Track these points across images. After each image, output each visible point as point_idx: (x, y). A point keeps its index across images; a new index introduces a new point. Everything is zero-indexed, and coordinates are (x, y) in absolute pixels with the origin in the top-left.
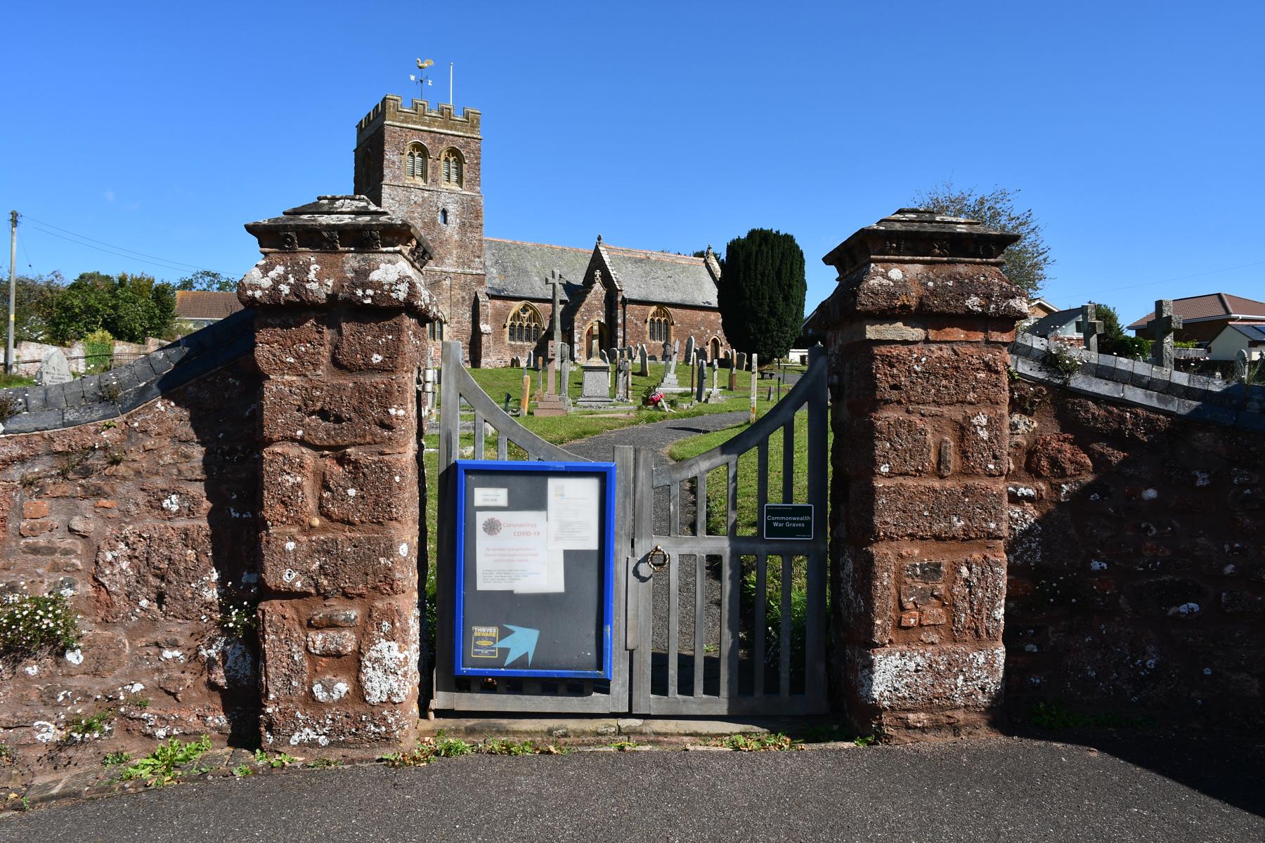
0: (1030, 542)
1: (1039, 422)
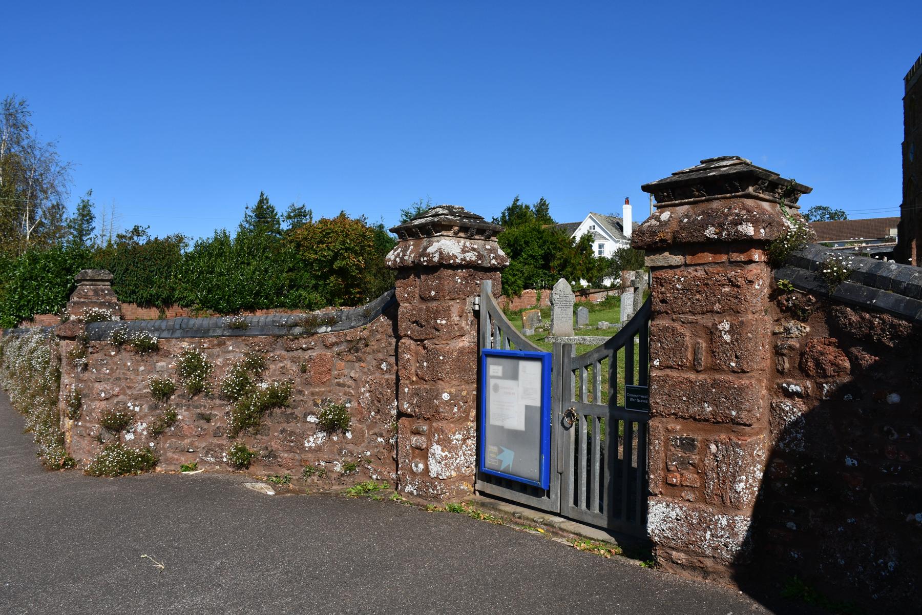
0: (797, 432)
1: (812, 327)
